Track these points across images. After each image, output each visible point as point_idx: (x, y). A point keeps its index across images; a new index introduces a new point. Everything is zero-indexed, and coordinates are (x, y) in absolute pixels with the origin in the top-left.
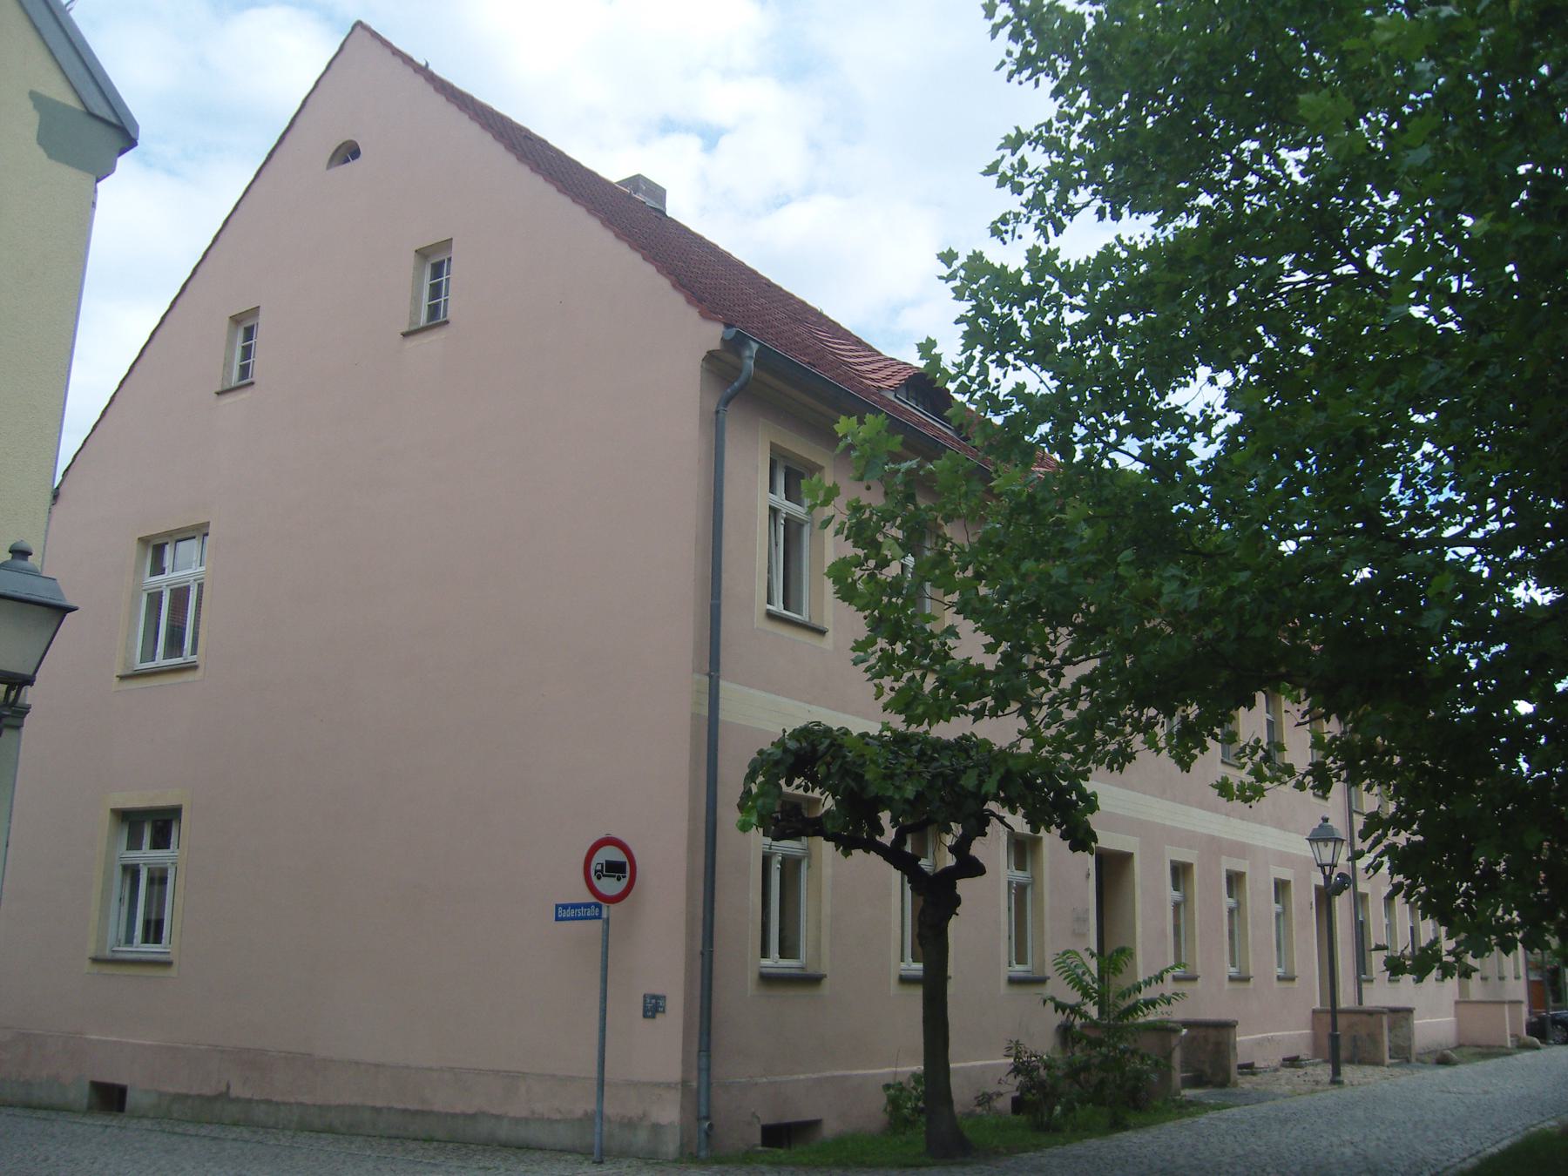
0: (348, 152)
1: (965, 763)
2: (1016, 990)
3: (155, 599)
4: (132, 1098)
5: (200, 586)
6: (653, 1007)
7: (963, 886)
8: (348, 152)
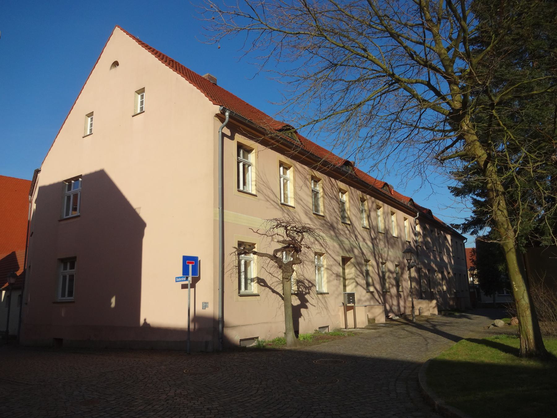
0: (116, 64)
7: (303, 311)
8: (116, 64)
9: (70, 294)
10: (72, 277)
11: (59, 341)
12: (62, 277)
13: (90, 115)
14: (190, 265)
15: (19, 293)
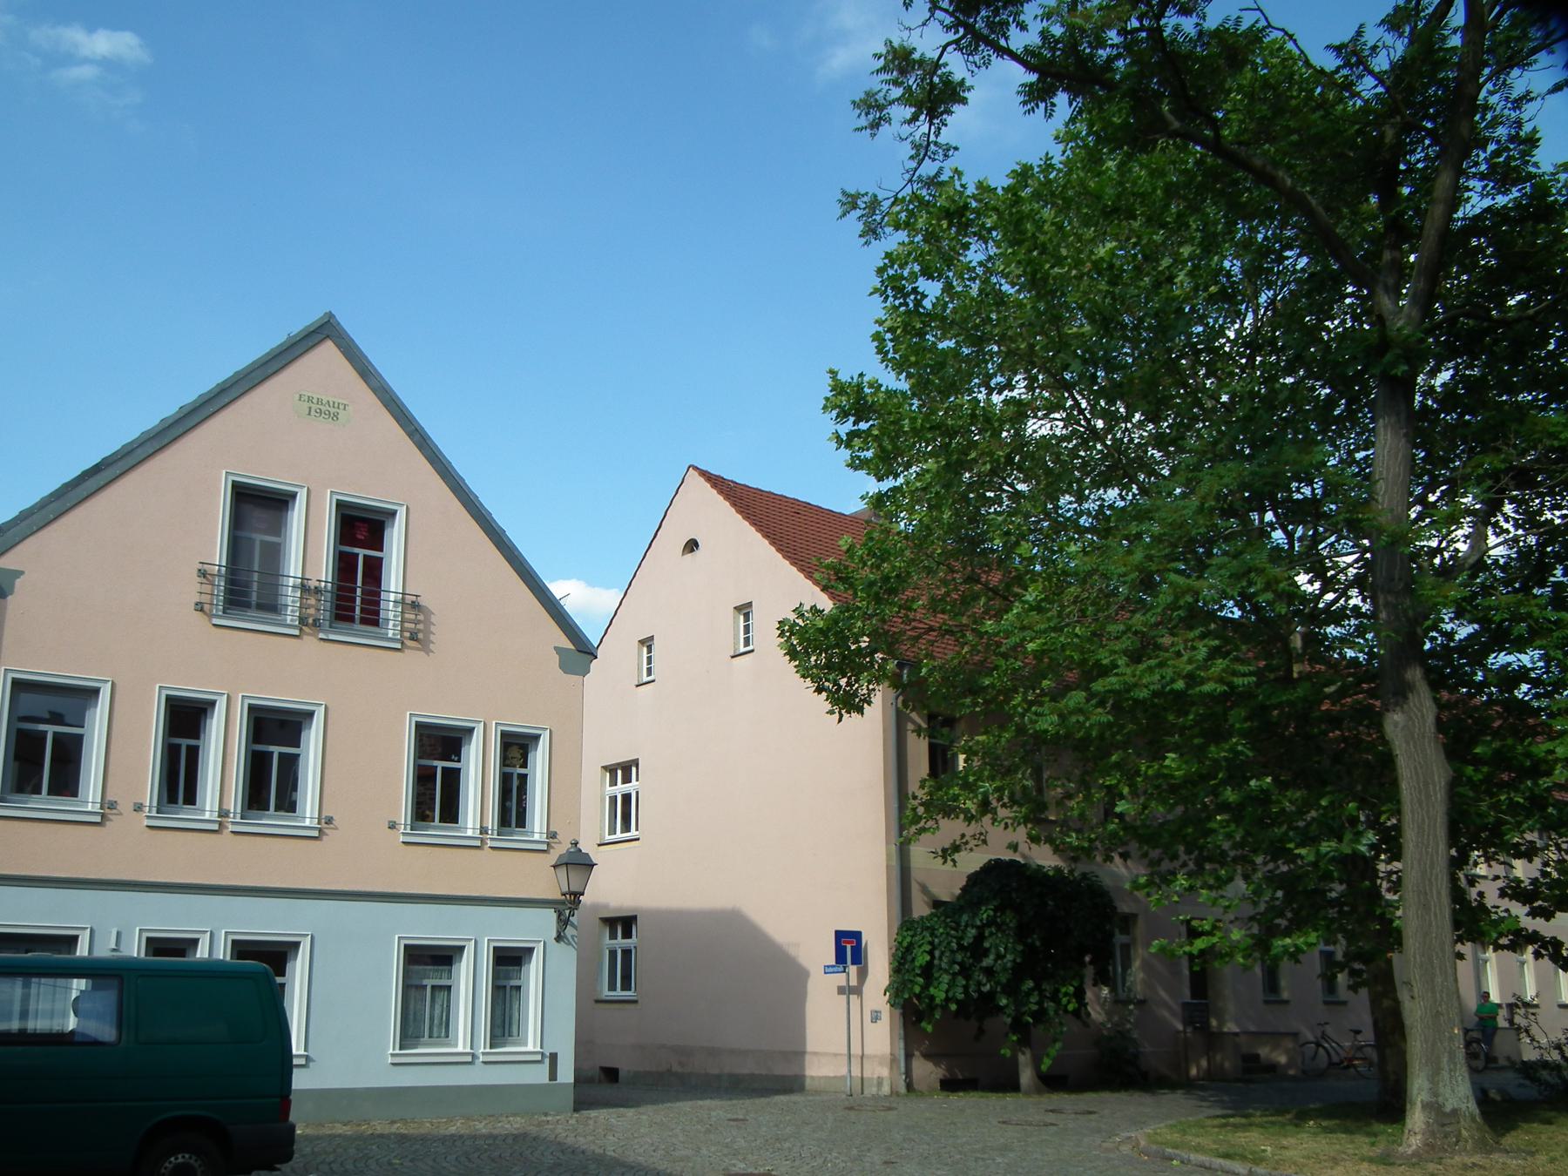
1: (1389, 867)
2: (1562, 1010)
3: (613, 800)
4: (621, 1074)
5: (637, 793)
6: (876, 1017)
13: (647, 642)
14: (849, 947)
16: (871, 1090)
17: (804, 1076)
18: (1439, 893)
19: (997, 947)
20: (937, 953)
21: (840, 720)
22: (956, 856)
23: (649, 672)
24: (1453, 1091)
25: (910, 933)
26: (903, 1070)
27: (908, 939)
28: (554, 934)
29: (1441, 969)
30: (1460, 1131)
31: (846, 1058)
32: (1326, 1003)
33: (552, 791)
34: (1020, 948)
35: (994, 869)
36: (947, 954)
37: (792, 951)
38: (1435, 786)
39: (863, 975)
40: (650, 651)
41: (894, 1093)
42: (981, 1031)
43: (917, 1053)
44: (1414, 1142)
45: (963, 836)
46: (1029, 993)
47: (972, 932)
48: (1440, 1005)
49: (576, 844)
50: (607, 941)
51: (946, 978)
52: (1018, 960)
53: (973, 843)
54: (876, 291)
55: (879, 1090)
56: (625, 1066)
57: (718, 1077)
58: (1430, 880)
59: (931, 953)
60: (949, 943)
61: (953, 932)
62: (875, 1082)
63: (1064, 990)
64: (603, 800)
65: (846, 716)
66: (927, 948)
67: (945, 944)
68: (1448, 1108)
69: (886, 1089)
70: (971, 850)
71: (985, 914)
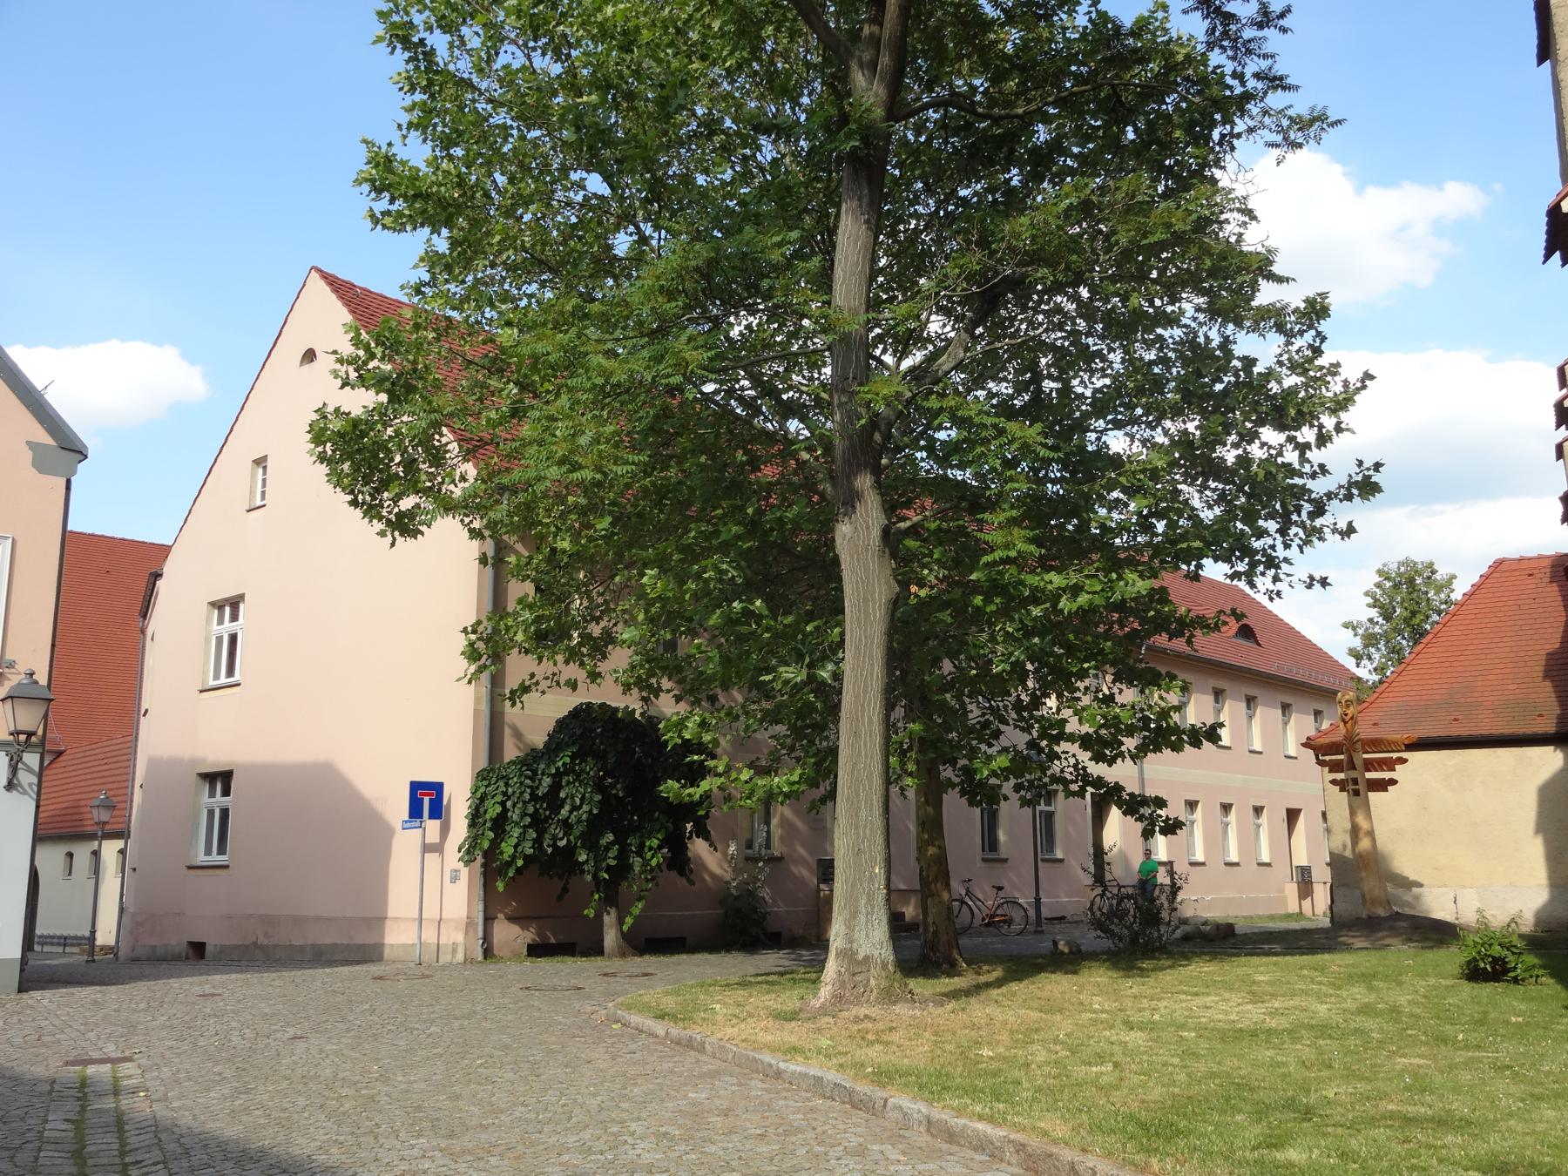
3: (219, 640)
4: (209, 949)
9: (221, 851)
10: (225, 813)
11: (198, 949)
12: (206, 812)
13: (261, 462)
14: (426, 800)
15: (120, 844)
16: (445, 958)
17: (383, 944)
18: (870, 720)
19: (573, 797)
20: (509, 804)
21: (393, 545)
22: (525, 698)
23: (263, 498)
24: (867, 936)
25: (485, 783)
26: (480, 934)
27: (482, 790)
28: (5, 782)
29: (866, 803)
30: (869, 980)
31: (417, 923)
32: (984, 860)
33: (11, 617)
34: (598, 798)
35: (581, 715)
36: (520, 805)
37: (379, 807)
38: (874, 604)
39: (445, 830)
40: (265, 473)
41: (469, 961)
42: (565, 890)
43: (501, 916)
44: (825, 992)
45: (532, 676)
46: (608, 848)
47: (547, 781)
48: (863, 842)
49: (31, 675)
50: (206, 799)
51: (516, 832)
52: (595, 812)
53: (544, 684)
54: (379, 40)
55: (453, 957)
56: (212, 941)
57: (302, 948)
58: (863, 706)
59: (503, 804)
60: (522, 793)
61: (528, 781)
62: (450, 949)
63: (648, 844)
64: (207, 640)
65: (400, 540)
66: (499, 798)
67: (517, 795)
68: (860, 957)
69: (460, 957)
70: (543, 693)
71: (563, 760)
